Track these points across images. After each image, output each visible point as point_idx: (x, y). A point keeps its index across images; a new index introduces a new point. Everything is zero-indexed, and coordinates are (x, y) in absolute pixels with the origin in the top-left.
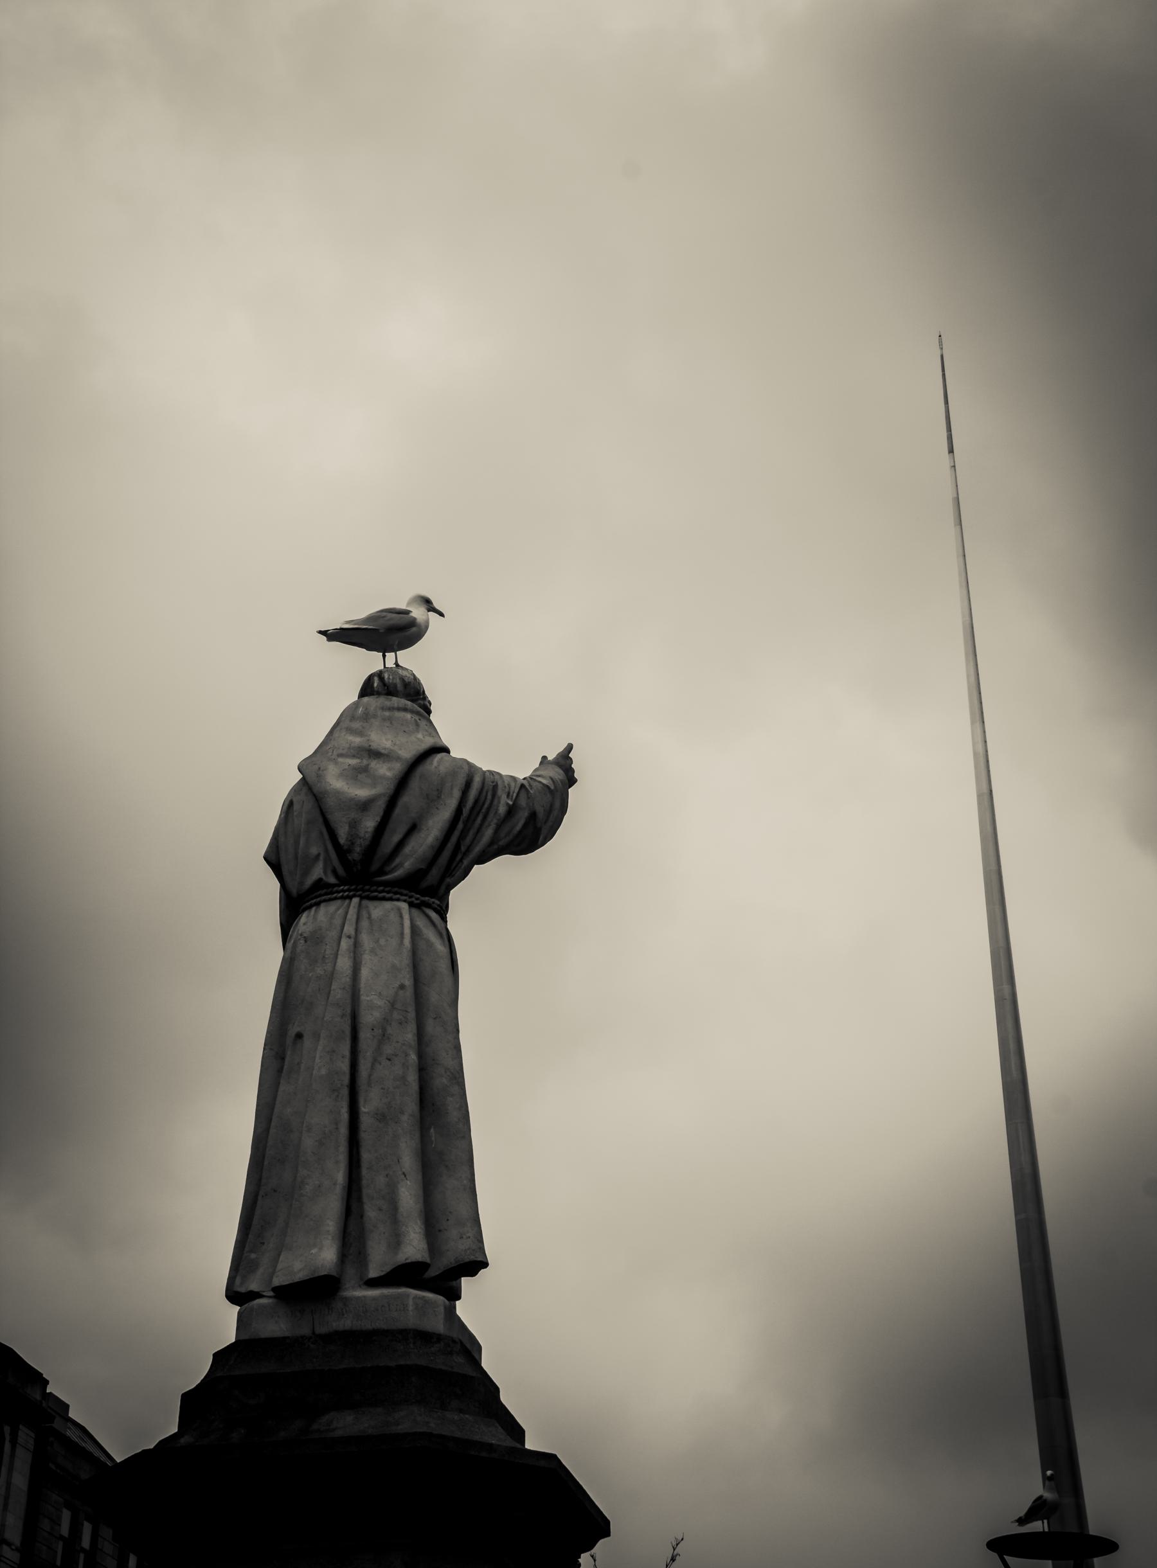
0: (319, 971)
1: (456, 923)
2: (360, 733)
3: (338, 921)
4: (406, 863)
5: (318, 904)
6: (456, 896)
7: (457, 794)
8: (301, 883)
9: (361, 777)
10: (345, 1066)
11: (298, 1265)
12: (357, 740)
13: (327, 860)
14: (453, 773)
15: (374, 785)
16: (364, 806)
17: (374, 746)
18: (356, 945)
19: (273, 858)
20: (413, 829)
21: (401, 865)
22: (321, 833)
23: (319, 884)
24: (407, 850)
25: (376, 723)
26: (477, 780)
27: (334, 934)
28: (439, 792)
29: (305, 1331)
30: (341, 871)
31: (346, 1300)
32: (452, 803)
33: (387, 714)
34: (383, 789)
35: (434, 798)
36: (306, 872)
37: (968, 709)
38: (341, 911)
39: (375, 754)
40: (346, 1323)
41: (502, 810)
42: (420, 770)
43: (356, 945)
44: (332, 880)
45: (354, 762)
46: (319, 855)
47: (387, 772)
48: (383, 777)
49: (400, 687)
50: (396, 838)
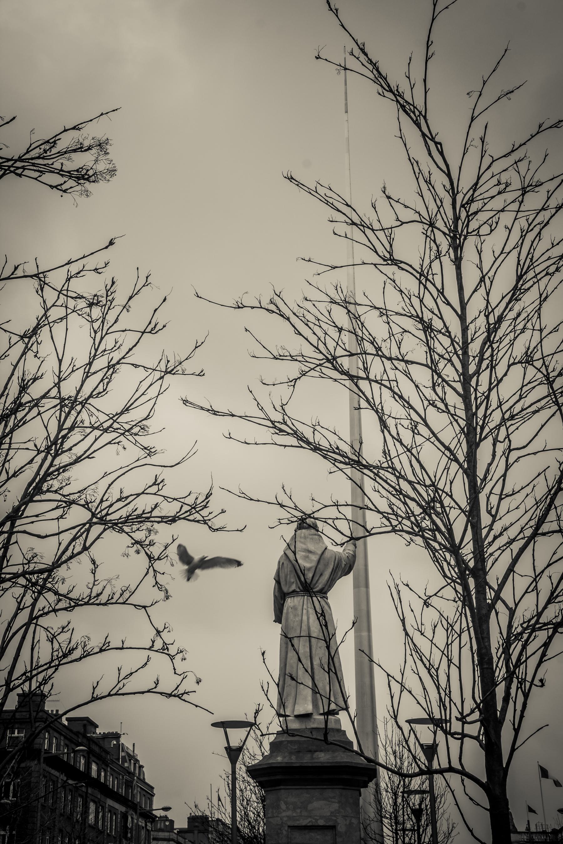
0: (297, 619)
1: (329, 601)
2: (304, 544)
3: (301, 604)
4: (319, 586)
5: (294, 597)
6: (329, 594)
7: (333, 564)
8: (288, 590)
9: (307, 559)
10: (308, 650)
11: (301, 709)
12: (304, 546)
13: (297, 583)
14: (331, 557)
15: (311, 563)
16: (309, 569)
17: (310, 549)
18: (308, 611)
19: (277, 579)
20: (321, 575)
21: (318, 586)
22: (295, 576)
23: (294, 591)
24: (320, 581)
25: (308, 540)
26: (337, 557)
27: (300, 608)
28: (328, 563)
29: (304, 727)
30: (301, 588)
31: (315, 719)
32: (331, 567)
33: (311, 537)
34: (313, 564)
35: (326, 565)
36: (290, 587)
37: (518, 562)
38: (302, 600)
39: (310, 552)
40: (315, 726)
41: (343, 566)
42: (323, 556)
43: (308, 611)
44: (298, 590)
45: (304, 554)
46: (293, 582)
47: (315, 558)
48: (313, 560)
49: (312, 525)
50: (317, 579)
